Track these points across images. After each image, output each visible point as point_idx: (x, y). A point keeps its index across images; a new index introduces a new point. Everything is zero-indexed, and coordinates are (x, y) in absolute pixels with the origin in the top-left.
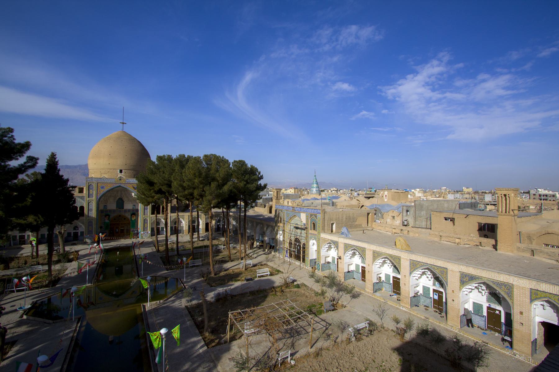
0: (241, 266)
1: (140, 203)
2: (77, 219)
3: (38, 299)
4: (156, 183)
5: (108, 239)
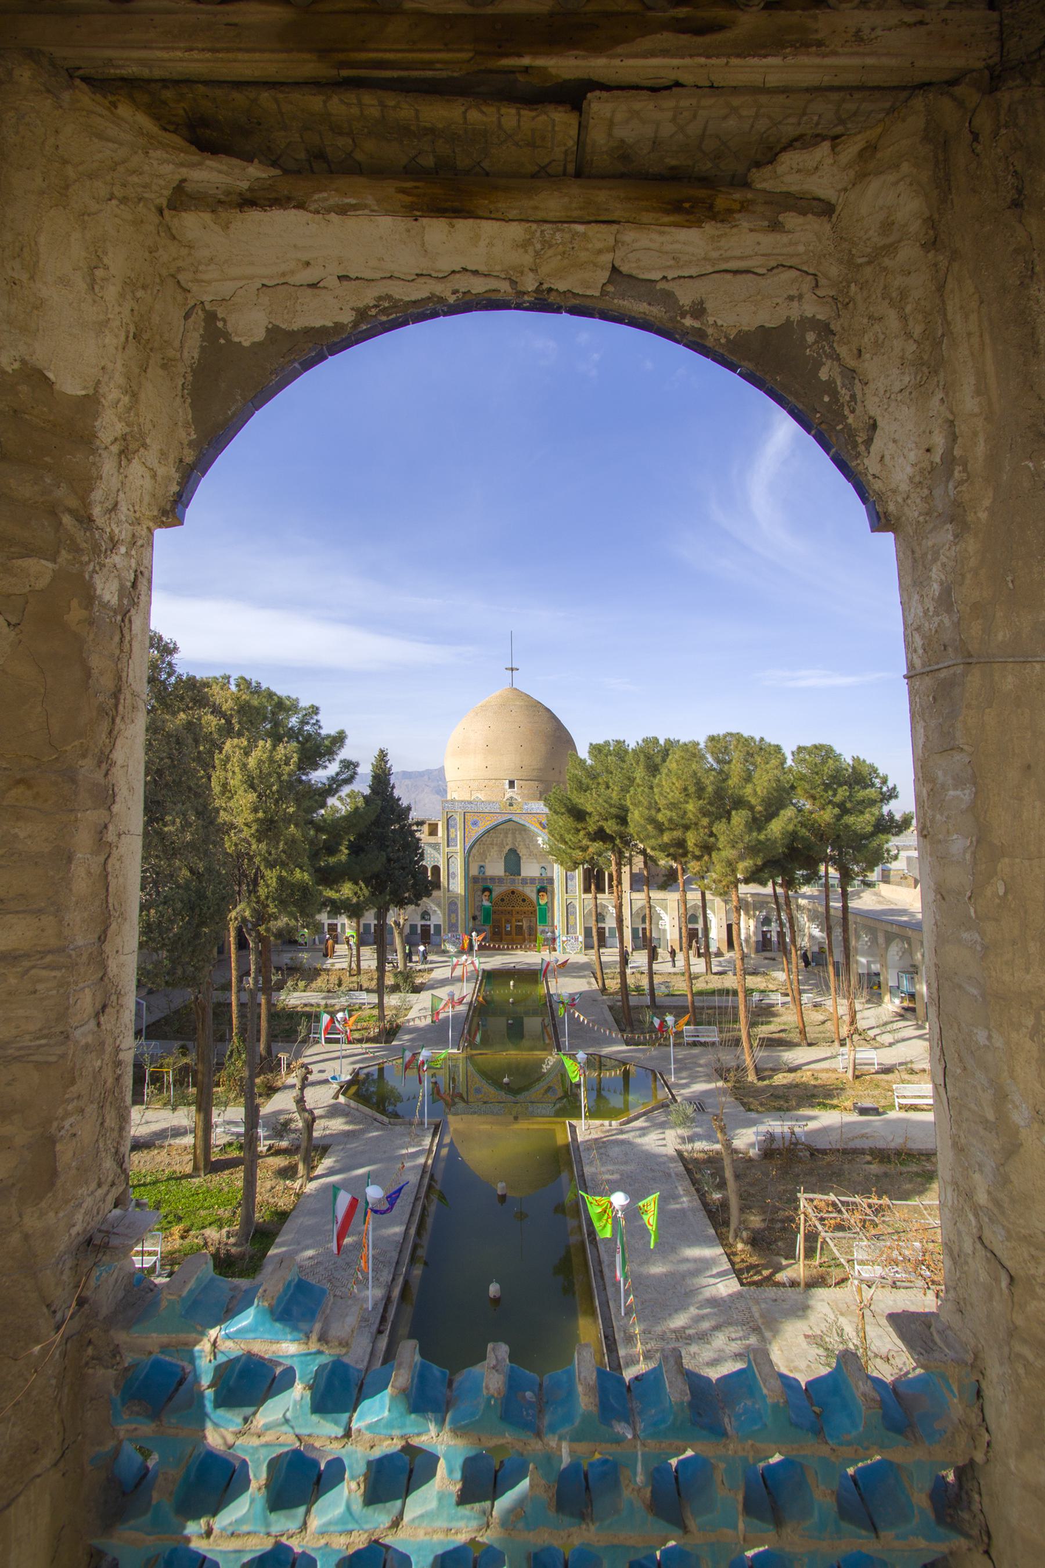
0: (839, 1064)
1: (556, 861)
2: (429, 895)
3: (361, 1065)
4: (590, 814)
5: (488, 948)
